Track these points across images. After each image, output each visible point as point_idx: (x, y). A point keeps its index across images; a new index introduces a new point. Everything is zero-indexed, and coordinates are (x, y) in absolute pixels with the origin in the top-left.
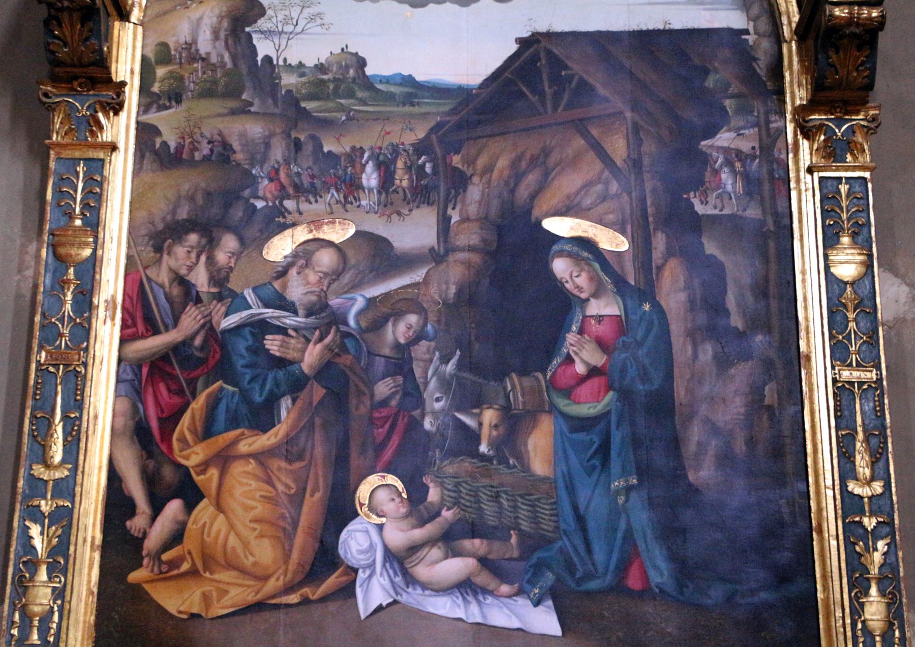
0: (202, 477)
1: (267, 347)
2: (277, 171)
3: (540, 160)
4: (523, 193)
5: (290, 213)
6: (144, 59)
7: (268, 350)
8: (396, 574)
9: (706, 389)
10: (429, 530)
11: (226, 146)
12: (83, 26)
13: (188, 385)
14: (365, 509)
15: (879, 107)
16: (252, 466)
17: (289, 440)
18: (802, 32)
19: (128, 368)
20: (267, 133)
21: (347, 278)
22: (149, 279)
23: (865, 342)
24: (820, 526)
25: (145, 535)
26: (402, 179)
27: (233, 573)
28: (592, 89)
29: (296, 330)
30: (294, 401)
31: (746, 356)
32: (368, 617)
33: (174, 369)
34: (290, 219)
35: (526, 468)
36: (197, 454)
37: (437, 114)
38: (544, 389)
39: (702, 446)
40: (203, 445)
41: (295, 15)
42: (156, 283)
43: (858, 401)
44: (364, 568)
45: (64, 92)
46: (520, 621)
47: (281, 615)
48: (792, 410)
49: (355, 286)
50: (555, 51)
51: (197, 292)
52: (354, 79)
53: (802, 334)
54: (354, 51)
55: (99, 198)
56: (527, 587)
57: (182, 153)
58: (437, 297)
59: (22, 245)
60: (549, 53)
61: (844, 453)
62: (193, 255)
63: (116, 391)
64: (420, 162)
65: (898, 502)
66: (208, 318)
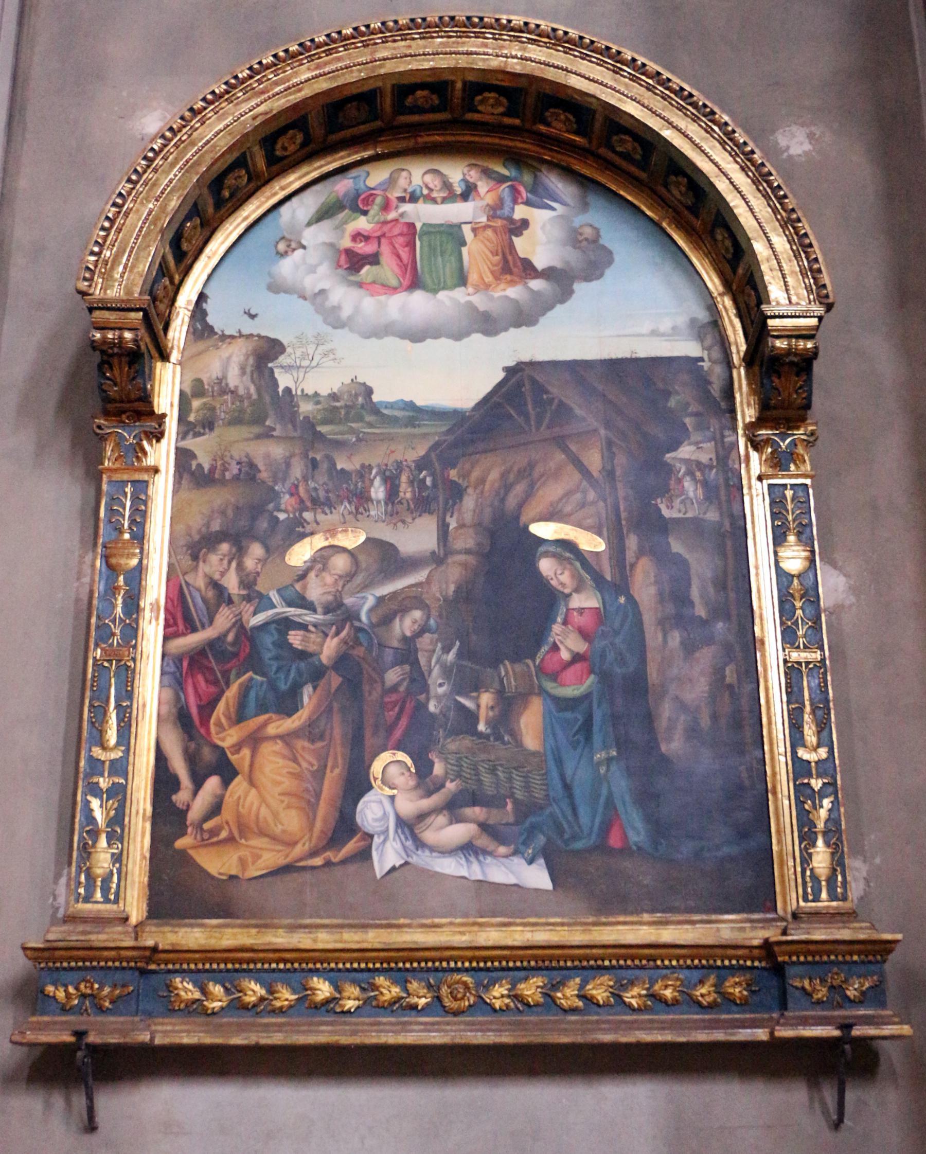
0: (236, 756)
1: (290, 641)
2: (296, 487)
3: (526, 472)
4: (512, 502)
5: (308, 523)
6: (182, 394)
7: (291, 645)
8: (407, 838)
9: (675, 671)
10: (436, 799)
11: (252, 465)
12: (130, 368)
13: (223, 676)
14: (379, 782)
15: (816, 424)
16: (279, 746)
17: (311, 724)
18: (750, 360)
19: (171, 662)
20: (287, 454)
21: (359, 579)
22: (187, 584)
23: (810, 627)
24: (774, 787)
25: (188, 807)
26: (406, 492)
27: (265, 840)
28: (571, 410)
29: (315, 626)
30: (315, 688)
31: (709, 641)
32: (383, 877)
33: (210, 662)
34: (308, 529)
35: (519, 744)
36: (232, 736)
37: (436, 434)
38: (534, 673)
39: (672, 722)
40: (237, 728)
41: (311, 352)
42: (193, 587)
43: (805, 678)
44: (379, 835)
45: (115, 424)
46: (517, 878)
47: (308, 876)
48: (749, 687)
49: (365, 587)
50: (538, 378)
51: (229, 594)
52: (362, 406)
53: (757, 621)
54: (362, 381)
55: (144, 514)
56: (522, 848)
57: (214, 473)
58: (438, 595)
59: (80, 556)
60: (534, 381)
61: (794, 724)
62: (225, 562)
63: (161, 682)
64: (422, 476)
65: (840, 766)
66: (239, 617)
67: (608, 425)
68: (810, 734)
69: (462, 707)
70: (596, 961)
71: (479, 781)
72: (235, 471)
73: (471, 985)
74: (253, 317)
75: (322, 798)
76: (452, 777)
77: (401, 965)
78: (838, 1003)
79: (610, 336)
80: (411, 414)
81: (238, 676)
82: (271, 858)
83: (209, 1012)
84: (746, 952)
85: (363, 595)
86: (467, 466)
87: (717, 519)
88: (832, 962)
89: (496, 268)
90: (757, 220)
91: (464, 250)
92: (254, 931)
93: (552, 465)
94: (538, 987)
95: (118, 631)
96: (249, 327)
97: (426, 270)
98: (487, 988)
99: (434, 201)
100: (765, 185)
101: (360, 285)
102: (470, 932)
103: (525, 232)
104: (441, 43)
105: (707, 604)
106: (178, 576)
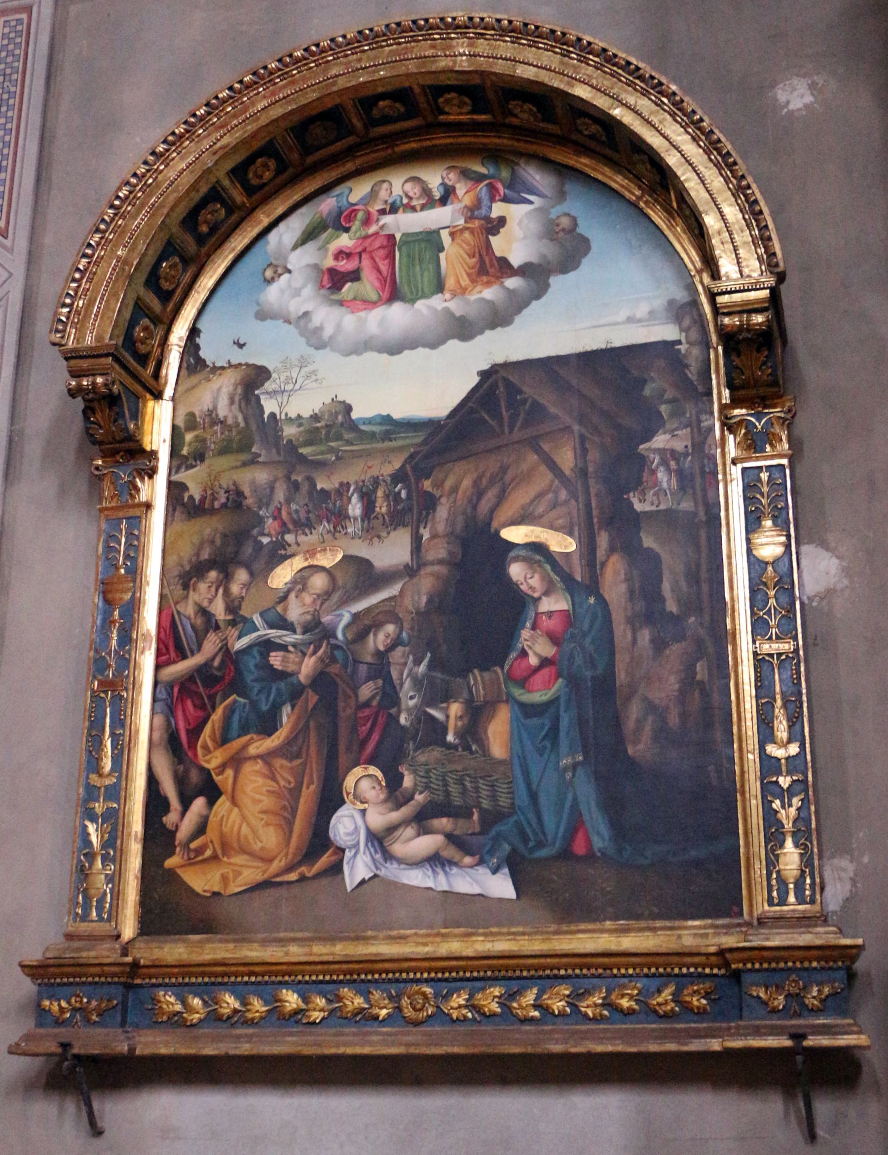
0: (220, 777)
2: (279, 510)
4: (484, 506)
5: (290, 545)
6: (174, 428)
7: (272, 666)
8: (376, 851)
11: (240, 494)
14: (351, 797)
16: (259, 765)
17: (289, 742)
19: (163, 689)
20: (272, 479)
21: (335, 597)
22: (178, 612)
23: (783, 616)
24: (743, 786)
26: (382, 507)
27: (245, 857)
29: (294, 646)
30: (293, 707)
31: (680, 637)
33: (198, 688)
34: (290, 551)
36: (217, 758)
37: (408, 446)
40: (221, 750)
41: (294, 375)
43: (776, 671)
44: (350, 848)
47: (283, 891)
49: (345, 602)
50: (511, 379)
52: (342, 424)
55: (137, 548)
58: (410, 608)
61: (764, 720)
62: (213, 589)
64: (397, 489)
67: (582, 419)
68: (781, 730)
69: (433, 718)
70: (551, 970)
71: (447, 793)
72: (223, 500)
73: (430, 996)
74: (241, 346)
75: (299, 812)
76: (420, 788)
77: (363, 976)
78: (795, 1012)
79: (585, 329)
80: (388, 428)
81: (224, 699)
82: (251, 874)
83: (188, 1023)
84: (703, 959)
85: (338, 612)
86: (441, 476)
87: (693, 509)
88: (790, 969)
89: (473, 271)
90: (708, 191)
91: (442, 256)
92: (231, 946)
93: (525, 467)
94: (495, 997)
95: (113, 664)
96: (238, 357)
97: (404, 281)
98: (447, 997)
99: (413, 209)
100: (715, 153)
101: (341, 303)
102: (432, 943)
103: (501, 230)
104: (391, 51)
105: (679, 601)
106: (170, 607)
